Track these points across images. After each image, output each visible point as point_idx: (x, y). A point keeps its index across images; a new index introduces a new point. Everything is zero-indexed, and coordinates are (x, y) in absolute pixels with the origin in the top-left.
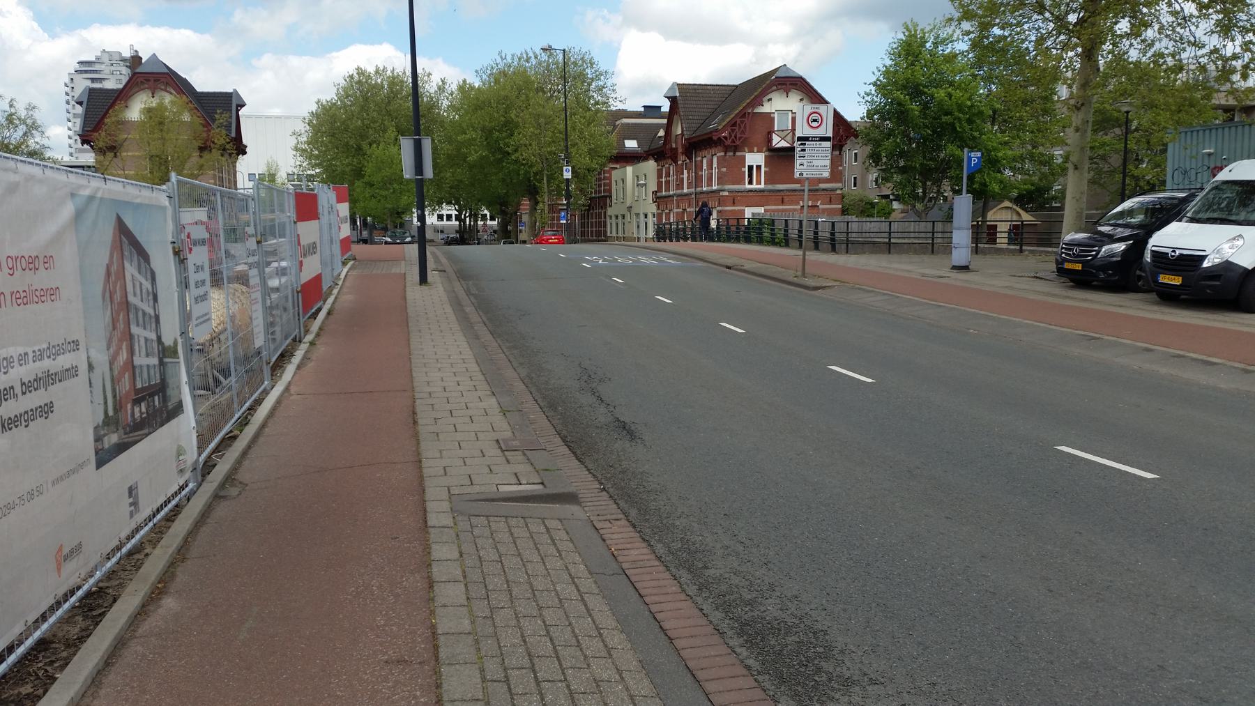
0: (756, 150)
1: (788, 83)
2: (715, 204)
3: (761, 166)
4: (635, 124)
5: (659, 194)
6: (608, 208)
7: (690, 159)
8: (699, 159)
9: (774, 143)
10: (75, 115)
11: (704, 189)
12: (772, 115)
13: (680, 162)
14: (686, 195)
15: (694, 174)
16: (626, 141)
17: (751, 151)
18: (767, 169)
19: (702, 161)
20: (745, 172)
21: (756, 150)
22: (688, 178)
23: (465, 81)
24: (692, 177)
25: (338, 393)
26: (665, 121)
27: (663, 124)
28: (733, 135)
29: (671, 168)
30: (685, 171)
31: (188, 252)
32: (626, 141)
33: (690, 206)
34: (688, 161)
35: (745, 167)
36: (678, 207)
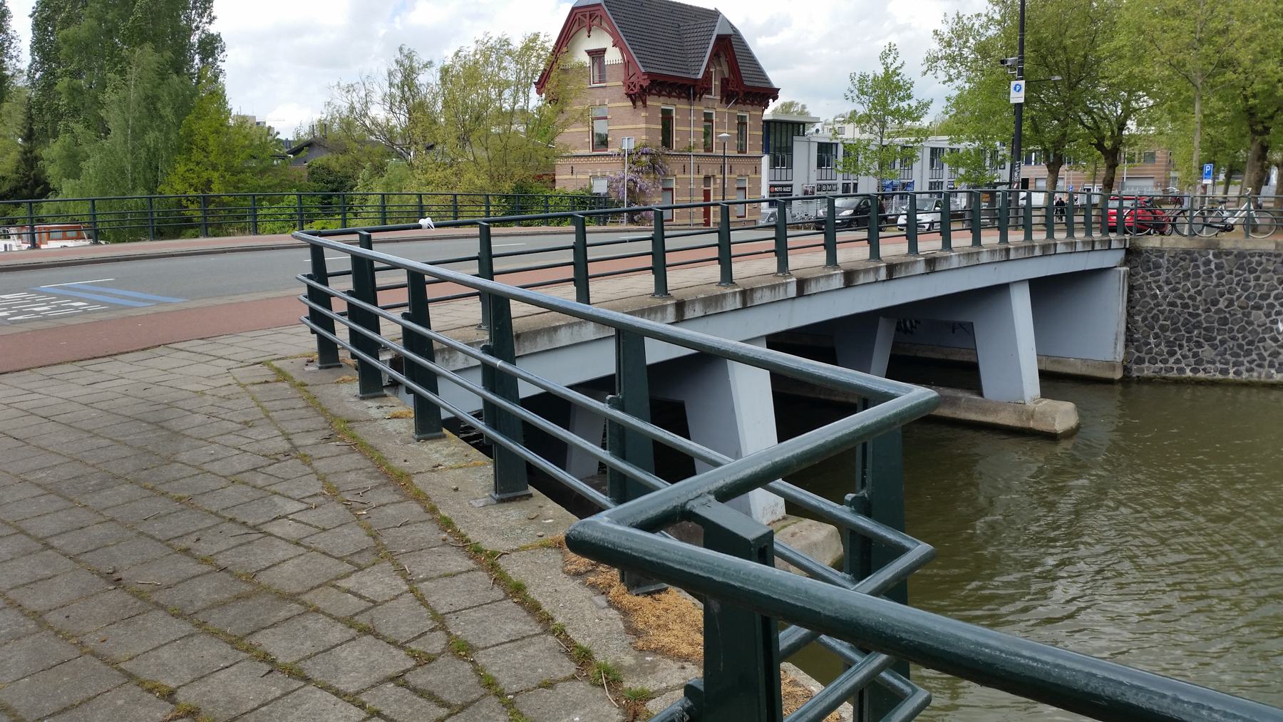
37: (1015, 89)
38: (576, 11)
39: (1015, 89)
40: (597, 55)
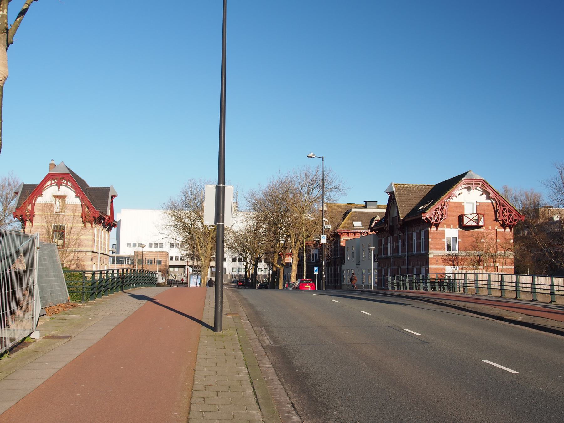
0: (452, 226)
1: (473, 183)
2: (400, 265)
3: (456, 237)
4: (360, 212)
5: (379, 256)
6: (342, 265)
7: (404, 233)
8: (410, 233)
9: (465, 223)
10: (251, 218)
11: (415, 253)
12: (463, 204)
13: (395, 235)
14: (401, 257)
15: (406, 243)
16: (354, 223)
17: (449, 227)
18: (443, 240)
19: (412, 234)
20: (444, 241)
21: (452, 226)
22: (402, 245)
23: (75, 197)
24: (405, 244)
25: (28, 370)
26: (385, 211)
27: (383, 213)
28: (511, 218)
29: (389, 239)
30: (400, 241)
31: (388, 290)
32: (354, 223)
33: (404, 264)
34: (402, 234)
35: (444, 238)
36: (394, 265)
37: (323, 238)
38: (50, 175)
39: (323, 238)
40: (62, 198)
